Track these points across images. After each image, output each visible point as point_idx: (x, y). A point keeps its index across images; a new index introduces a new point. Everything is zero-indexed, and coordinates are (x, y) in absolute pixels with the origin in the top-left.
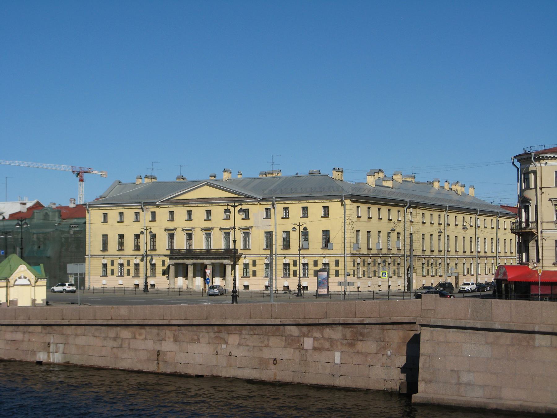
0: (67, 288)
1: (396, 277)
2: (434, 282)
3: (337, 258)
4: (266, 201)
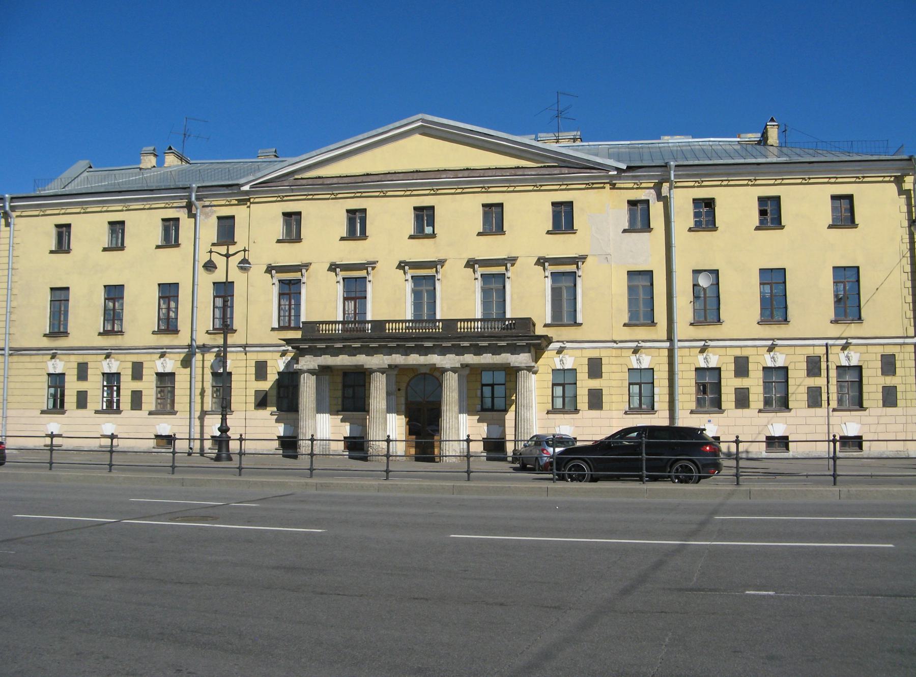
0: (551, 450)
3: (889, 350)
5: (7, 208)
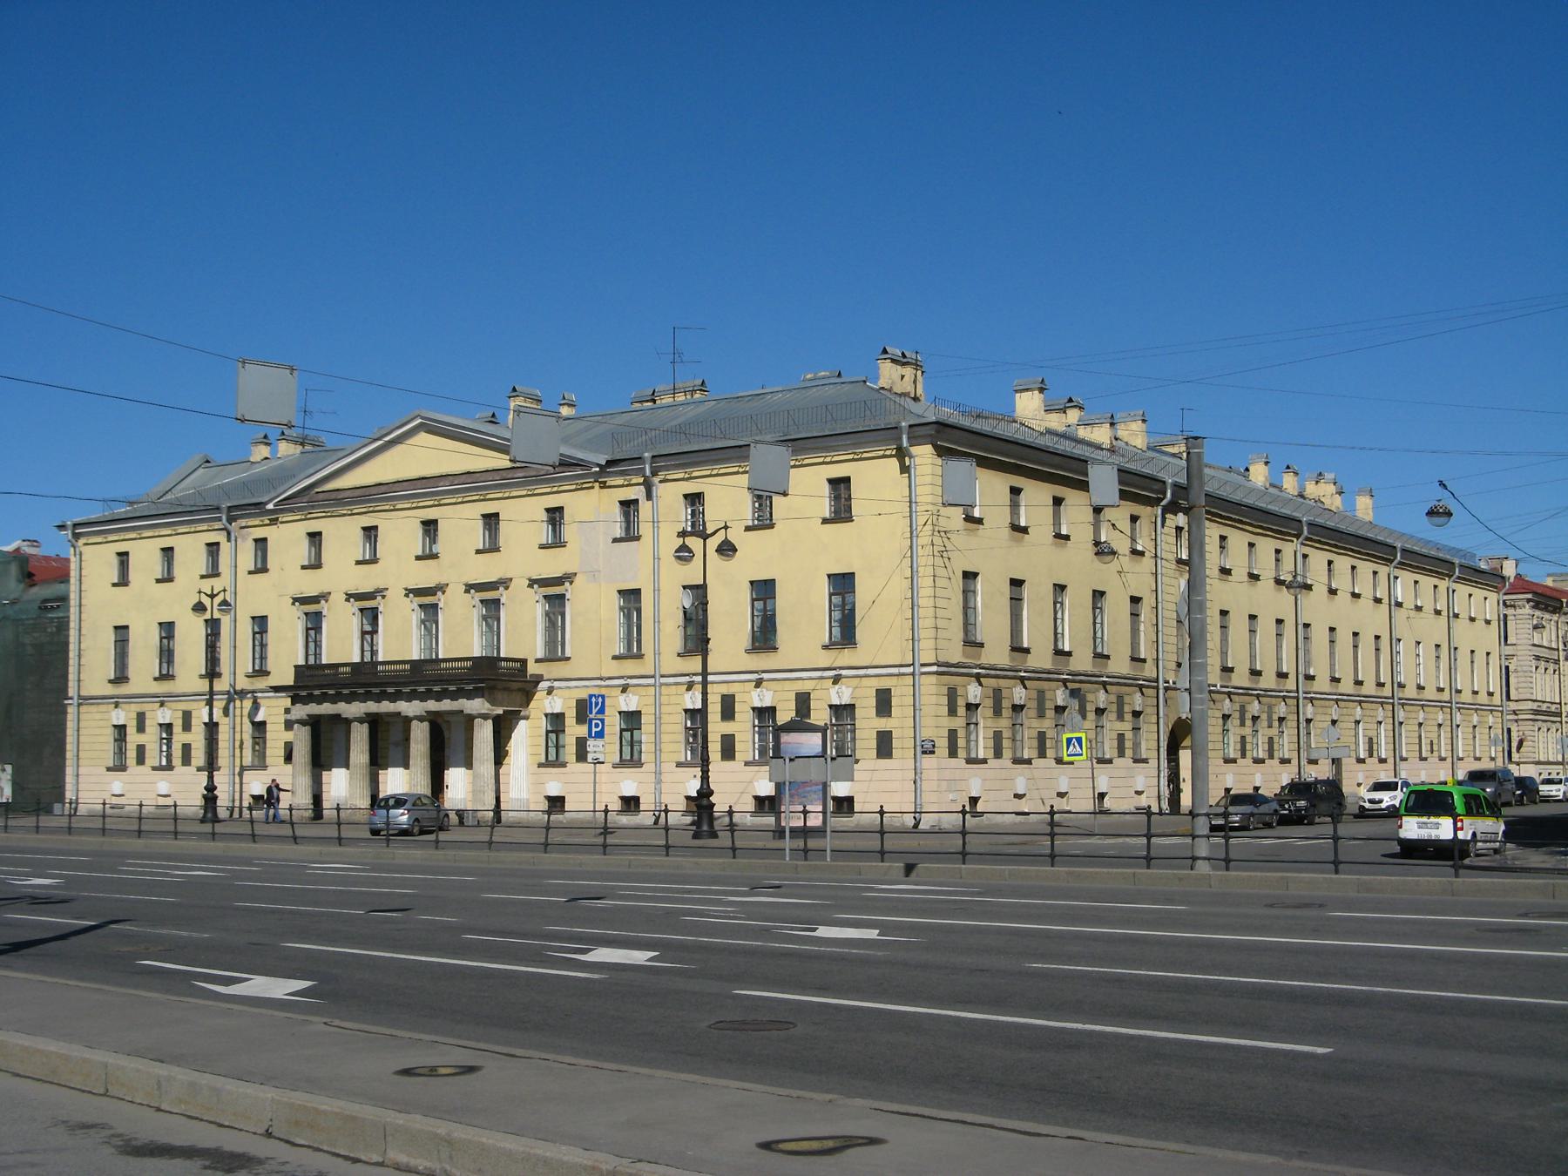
1: (1127, 761)
2: (1271, 780)
3: (885, 683)
4: (623, 473)
5: (648, 473)
